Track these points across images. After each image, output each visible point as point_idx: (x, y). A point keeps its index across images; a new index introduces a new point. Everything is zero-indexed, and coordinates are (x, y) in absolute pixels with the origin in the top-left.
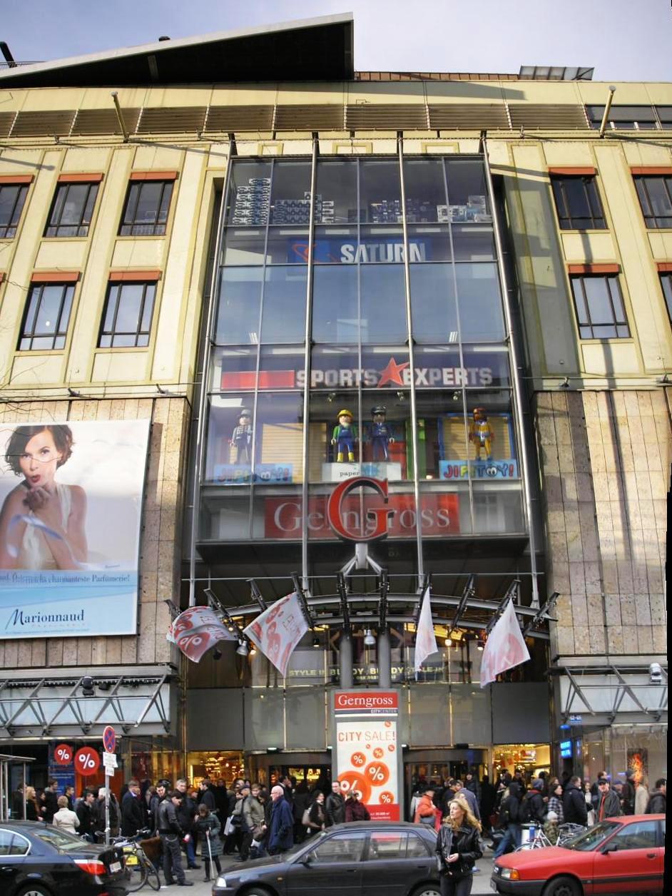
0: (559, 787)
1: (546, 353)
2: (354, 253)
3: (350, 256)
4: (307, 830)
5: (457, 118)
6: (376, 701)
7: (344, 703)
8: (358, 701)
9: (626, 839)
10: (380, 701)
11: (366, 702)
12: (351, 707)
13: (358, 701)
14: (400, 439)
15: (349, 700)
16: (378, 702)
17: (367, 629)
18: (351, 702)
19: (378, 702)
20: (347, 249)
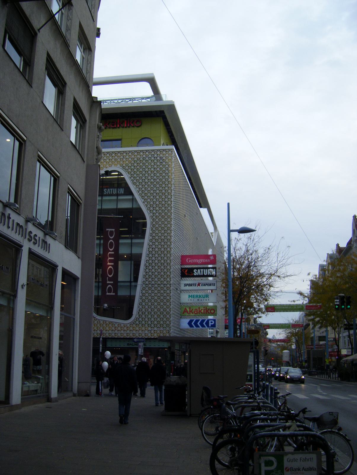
0: (36, 323)
1: (60, 244)
2: (197, 272)
3: (196, 273)
4: (277, 376)
5: (193, 213)
6: (202, 260)
7: (189, 261)
8: (195, 261)
9: (115, 126)
10: (204, 261)
11: (198, 261)
12: (200, 268)
13: (195, 261)
14: (265, 304)
15: (191, 260)
16: (203, 261)
17: (304, 366)
18: (192, 261)
19: (203, 261)
20: (195, 274)
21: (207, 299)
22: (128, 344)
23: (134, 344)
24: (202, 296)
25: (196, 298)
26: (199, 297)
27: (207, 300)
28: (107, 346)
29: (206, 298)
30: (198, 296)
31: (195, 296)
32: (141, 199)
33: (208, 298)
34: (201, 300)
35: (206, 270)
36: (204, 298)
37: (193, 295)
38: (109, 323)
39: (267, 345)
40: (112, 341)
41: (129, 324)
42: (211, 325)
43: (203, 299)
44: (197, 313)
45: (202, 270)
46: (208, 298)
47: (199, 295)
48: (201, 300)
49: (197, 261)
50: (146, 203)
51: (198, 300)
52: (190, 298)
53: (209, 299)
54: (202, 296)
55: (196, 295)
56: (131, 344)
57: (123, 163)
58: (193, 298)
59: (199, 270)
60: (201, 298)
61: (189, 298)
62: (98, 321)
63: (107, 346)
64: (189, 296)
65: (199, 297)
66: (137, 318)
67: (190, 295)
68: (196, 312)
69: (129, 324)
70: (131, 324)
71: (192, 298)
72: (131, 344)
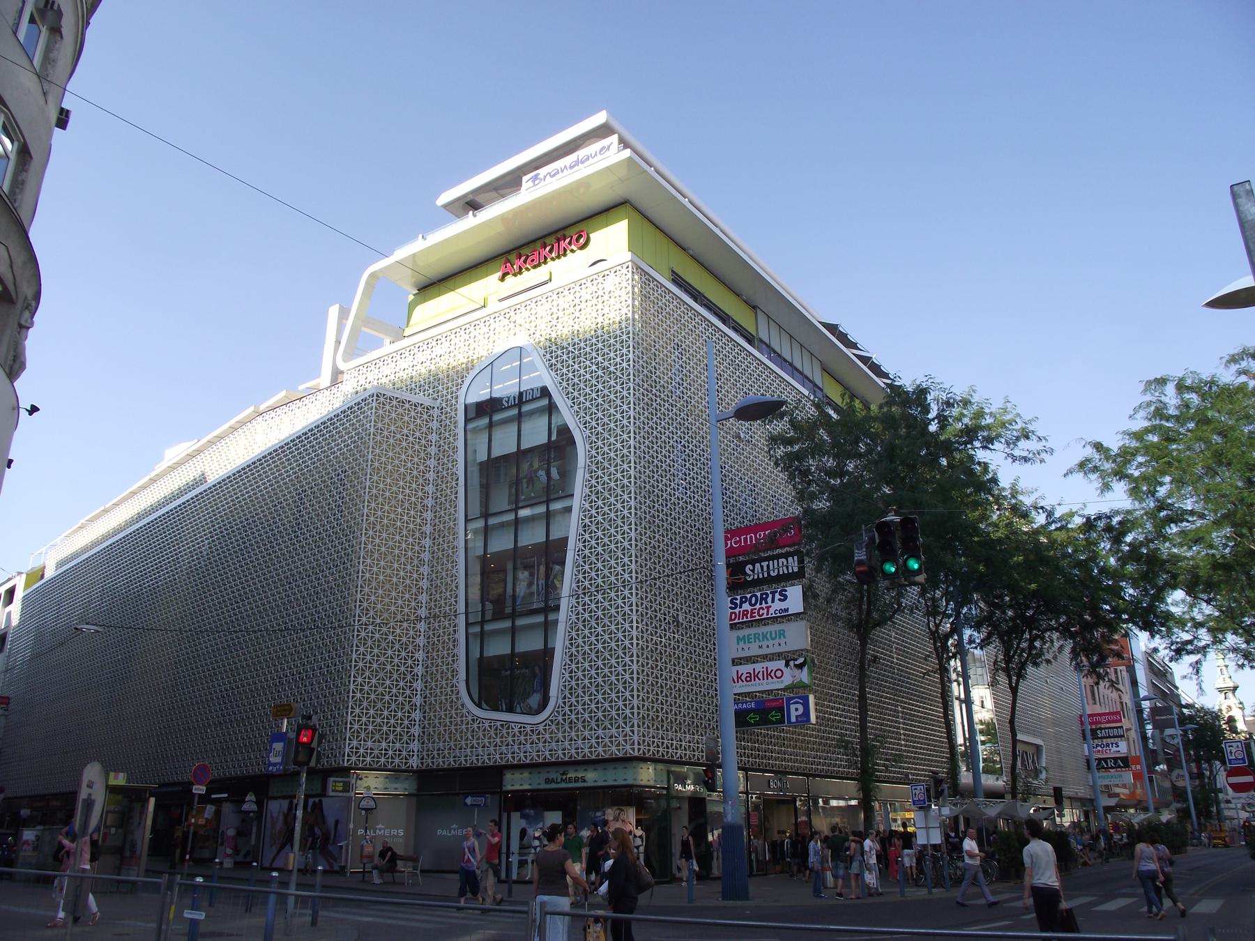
8: (746, 540)
13: (746, 540)
18: (736, 543)
21: (782, 641)
22: (547, 781)
23: (559, 780)
24: (768, 635)
25: (755, 642)
26: (761, 638)
27: (783, 644)
28: (504, 789)
29: (780, 638)
30: (759, 634)
31: (752, 637)
32: (567, 400)
33: (784, 637)
34: (768, 646)
35: (776, 561)
36: (775, 639)
37: (748, 635)
38: (502, 725)
39: (282, 719)
40: (539, 773)
41: (544, 724)
42: (797, 717)
43: (770, 642)
44: (751, 681)
45: (765, 564)
46: (784, 637)
47: (763, 633)
48: (768, 646)
49: (751, 541)
50: (576, 407)
51: (760, 647)
52: (741, 643)
53: (786, 640)
54: (768, 635)
55: (755, 634)
56: (553, 781)
57: (623, 346)
58: (749, 642)
59: (758, 565)
60: (768, 640)
61: (738, 644)
62: (479, 723)
63: (504, 789)
64: (738, 637)
65: (761, 638)
66: (559, 708)
67: (741, 637)
68: (748, 679)
69: (544, 724)
70: (551, 720)
71: (745, 643)
72: (553, 781)
